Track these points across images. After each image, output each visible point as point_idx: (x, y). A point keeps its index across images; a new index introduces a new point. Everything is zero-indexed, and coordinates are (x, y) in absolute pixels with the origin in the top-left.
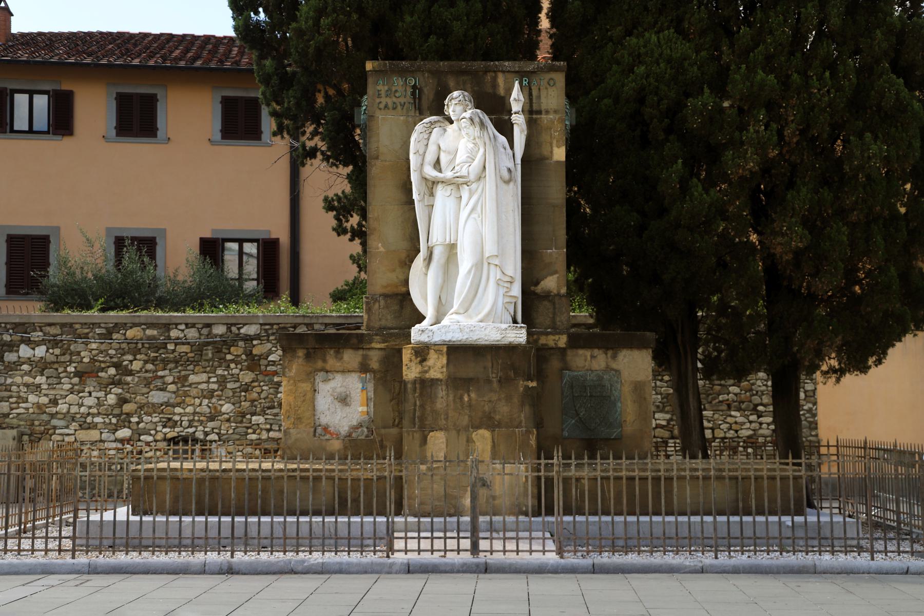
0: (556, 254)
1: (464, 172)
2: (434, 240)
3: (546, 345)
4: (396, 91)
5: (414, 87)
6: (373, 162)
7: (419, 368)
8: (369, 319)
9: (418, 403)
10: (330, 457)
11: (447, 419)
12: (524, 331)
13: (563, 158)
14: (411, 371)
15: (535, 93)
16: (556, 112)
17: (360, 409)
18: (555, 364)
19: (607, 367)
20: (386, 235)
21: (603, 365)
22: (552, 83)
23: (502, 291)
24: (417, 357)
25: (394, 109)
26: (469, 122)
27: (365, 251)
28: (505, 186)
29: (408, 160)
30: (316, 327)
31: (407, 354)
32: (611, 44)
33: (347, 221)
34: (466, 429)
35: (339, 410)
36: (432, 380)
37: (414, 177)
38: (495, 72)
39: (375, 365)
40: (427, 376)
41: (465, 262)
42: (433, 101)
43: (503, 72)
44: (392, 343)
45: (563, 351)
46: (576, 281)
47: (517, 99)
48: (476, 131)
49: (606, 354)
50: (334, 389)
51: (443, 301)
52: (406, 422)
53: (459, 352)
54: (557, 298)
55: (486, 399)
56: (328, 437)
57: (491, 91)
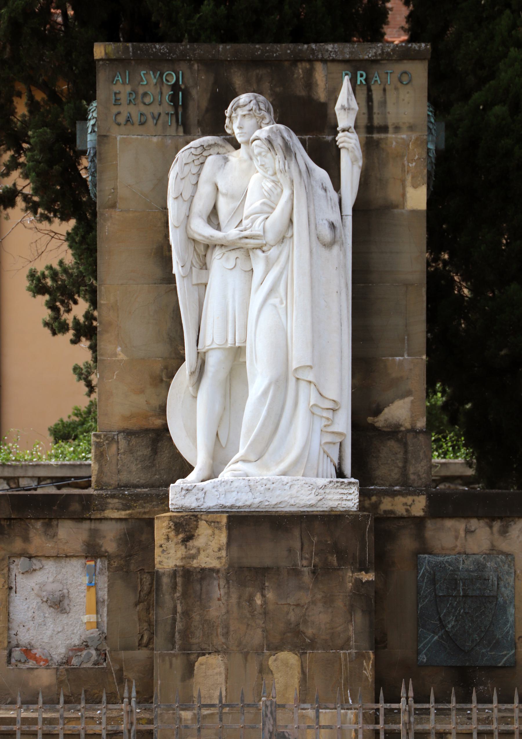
0: (409, 363)
1: (257, 229)
2: (208, 342)
3: (392, 512)
4: (145, 94)
5: (175, 87)
6: (107, 213)
7: (181, 551)
8: (101, 471)
9: (179, 609)
10: (30, 701)
11: (226, 634)
13: (423, 206)
14: (168, 556)
15: (377, 96)
16: (411, 128)
17: (85, 618)
18: (406, 543)
19: (493, 548)
20: (128, 333)
21: (485, 546)
22: (405, 79)
23: (319, 424)
24: (177, 533)
25: (142, 124)
26: (265, 147)
27: (95, 360)
29: (165, 209)
30: (23, 483)
31: (161, 528)
32: (508, 12)
33: (69, 311)
34: (259, 651)
35: (49, 621)
36: (203, 570)
37: (175, 238)
38: (310, 61)
39: (110, 545)
40: (195, 563)
41: (259, 378)
42: (207, 110)
43: (324, 61)
44: (138, 511)
45: (419, 523)
46: (445, 406)
47: (346, 108)
48: (276, 161)
49: (491, 527)
50: (42, 586)
51: (223, 441)
52: (159, 640)
53: (244, 524)
54: (410, 436)
55: (291, 601)
56: (31, 664)
57: (302, 93)
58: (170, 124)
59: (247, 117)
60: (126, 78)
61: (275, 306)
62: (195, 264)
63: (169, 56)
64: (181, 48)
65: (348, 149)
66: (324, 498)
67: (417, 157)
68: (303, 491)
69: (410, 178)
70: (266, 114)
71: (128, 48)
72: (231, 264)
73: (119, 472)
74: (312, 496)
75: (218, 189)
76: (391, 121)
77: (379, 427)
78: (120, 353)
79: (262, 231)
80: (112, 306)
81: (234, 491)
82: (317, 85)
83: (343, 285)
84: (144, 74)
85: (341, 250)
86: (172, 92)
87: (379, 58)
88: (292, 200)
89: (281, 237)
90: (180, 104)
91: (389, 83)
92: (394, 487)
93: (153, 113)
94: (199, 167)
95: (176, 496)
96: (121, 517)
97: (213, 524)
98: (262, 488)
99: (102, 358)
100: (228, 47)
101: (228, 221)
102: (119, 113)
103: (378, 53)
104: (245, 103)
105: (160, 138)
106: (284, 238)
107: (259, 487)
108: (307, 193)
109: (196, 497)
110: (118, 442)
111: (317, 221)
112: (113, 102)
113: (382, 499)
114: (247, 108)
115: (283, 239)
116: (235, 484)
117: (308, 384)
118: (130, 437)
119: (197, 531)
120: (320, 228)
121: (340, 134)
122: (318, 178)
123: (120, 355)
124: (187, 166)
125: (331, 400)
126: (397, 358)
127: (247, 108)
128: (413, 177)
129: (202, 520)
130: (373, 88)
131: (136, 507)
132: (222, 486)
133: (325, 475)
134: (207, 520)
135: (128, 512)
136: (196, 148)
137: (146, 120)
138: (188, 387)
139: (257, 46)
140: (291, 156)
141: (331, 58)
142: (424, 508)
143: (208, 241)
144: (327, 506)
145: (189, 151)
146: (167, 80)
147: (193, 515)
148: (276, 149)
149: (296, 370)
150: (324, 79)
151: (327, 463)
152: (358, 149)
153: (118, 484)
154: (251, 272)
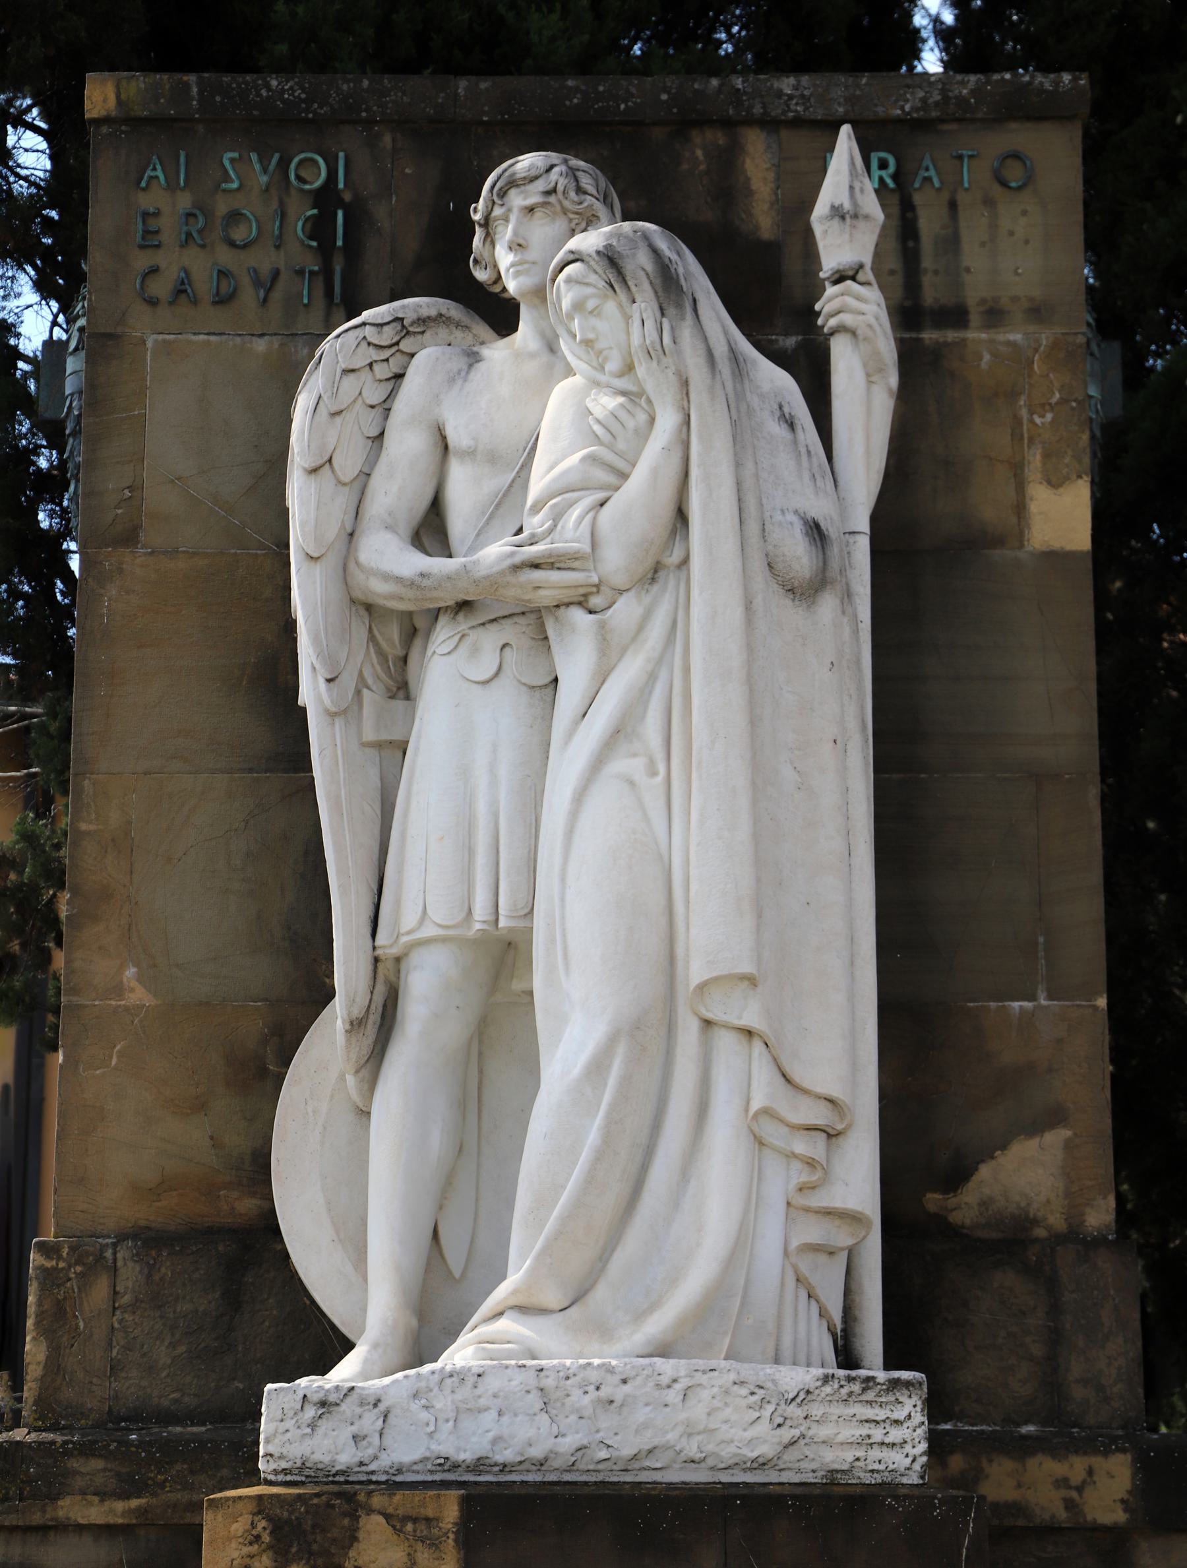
1: (571, 534)
2: (409, 919)
3: (1017, 1508)
4: (235, 217)
5: (326, 198)
12: (911, 1408)
15: (929, 223)
16: (1037, 313)
22: (1014, 173)
23: (780, 1182)
25: (222, 300)
28: (790, 613)
41: (574, 1024)
43: (770, 124)
47: (844, 209)
58: (306, 301)
59: (538, 214)
60: (178, 173)
61: (632, 783)
62: (370, 681)
63: (307, 110)
64: (345, 87)
65: (853, 333)
66: (803, 1436)
67: (1057, 395)
68: (729, 1410)
69: (1038, 457)
70: (599, 207)
71: (187, 85)
72: (486, 666)
73: (115, 1368)
74: (763, 1428)
75: (446, 447)
76: (975, 292)
77: (963, 1226)
78: (134, 984)
79: (588, 540)
80: (113, 840)
81: (487, 1409)
82: (750, 193)
83: (853, 724)
84: (232, 160)
85: (843, 612)
86: (315, 211)
87: (934, 114)
88: (686, 446)
89: (649, 563)
90: (340, 243)
91: (966, 185)
92: (1018, 1425)
93: (255, 271)
94: (389, 386)
95: (282, 1427)
96: (112, 1520)
97: (409, 1527)
98: (586, 1400)
99: (75, 999)
100: (483, 85)
101: (478, 535)
102: (154, 271)
103: (931, 101)
104: (533, 173)
105: (276, 342)
106: (657, 568)
107: (576, 1393)
108: (734, 424)
109: (354, 1429)
110: (116, 1270)
111: (767, 514)
112: (139, 239)
113: (985, 1463)
114: (541, 185)
115: (656, 571)
116: (492, 1384)
117: (744, 1039)
118: (153, 1253)
119: (352, 1553)
120: (776, 535)
121: (831, 290)
122: (766, 387)
123: (132, 990)
124: (352, 376)
125: (819, 1097)
126: (1016, 1004)
127: (541, 185)
128: (1046, 456)
129: (370, 1511)
130: (917, 199)
131: (162, 1485)
132: (447, 1392)
133: (802, 1357)
134: (390, 1510)
135: (134, 1503)
136: (382, 325)
137: (235, 290)
138: (342, 1078)
139: (570, 83)
140: (679, 306)
141: (791, 114)
142: (1126, 1497)
143: (410, 593)
144: (814, 1466)
145: (359, 333)
146: (299, 178)
147: (339, 1495)
148: (630, 283)
149: (702, 987)
150: (771, 176)
151: (809, 1320)
152: (885, 333)
153: (110, 1411)
154: (550, 690)
